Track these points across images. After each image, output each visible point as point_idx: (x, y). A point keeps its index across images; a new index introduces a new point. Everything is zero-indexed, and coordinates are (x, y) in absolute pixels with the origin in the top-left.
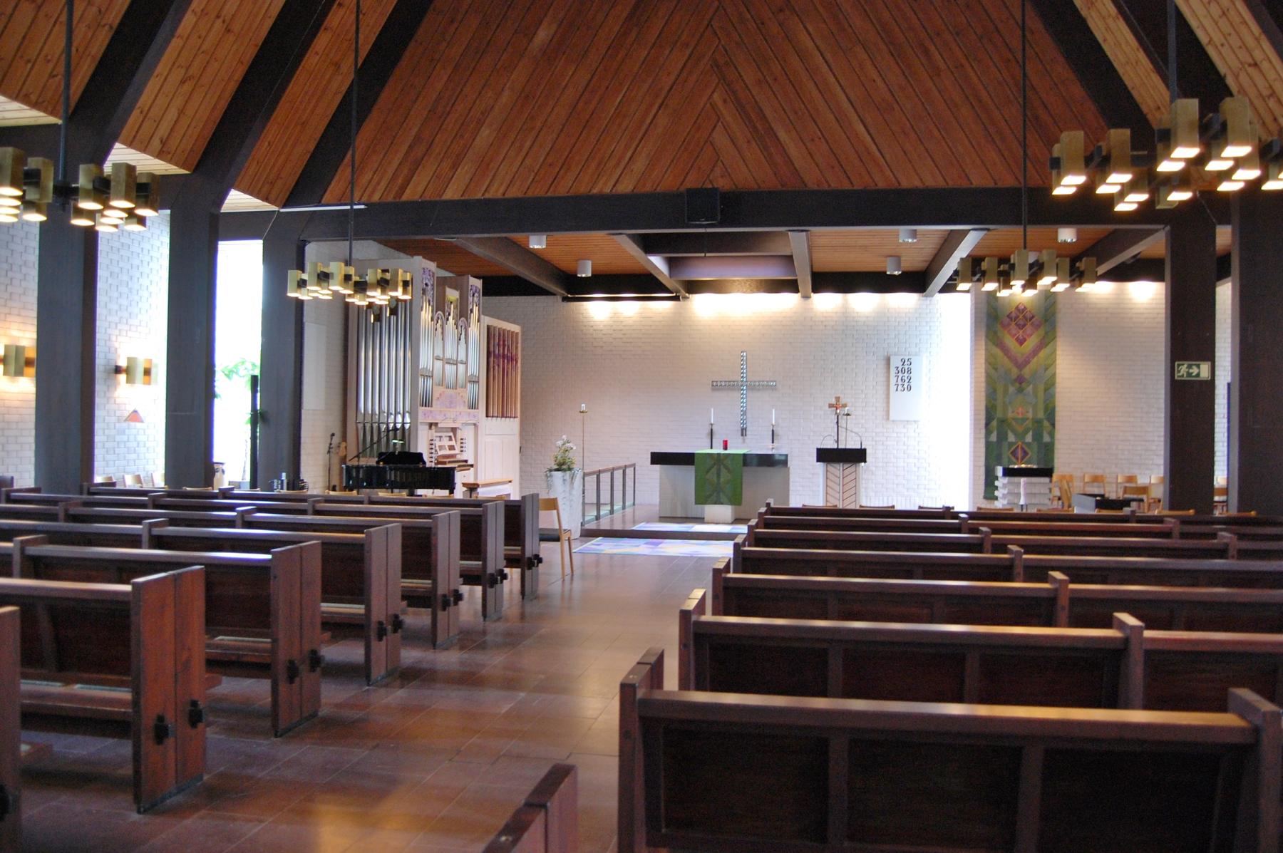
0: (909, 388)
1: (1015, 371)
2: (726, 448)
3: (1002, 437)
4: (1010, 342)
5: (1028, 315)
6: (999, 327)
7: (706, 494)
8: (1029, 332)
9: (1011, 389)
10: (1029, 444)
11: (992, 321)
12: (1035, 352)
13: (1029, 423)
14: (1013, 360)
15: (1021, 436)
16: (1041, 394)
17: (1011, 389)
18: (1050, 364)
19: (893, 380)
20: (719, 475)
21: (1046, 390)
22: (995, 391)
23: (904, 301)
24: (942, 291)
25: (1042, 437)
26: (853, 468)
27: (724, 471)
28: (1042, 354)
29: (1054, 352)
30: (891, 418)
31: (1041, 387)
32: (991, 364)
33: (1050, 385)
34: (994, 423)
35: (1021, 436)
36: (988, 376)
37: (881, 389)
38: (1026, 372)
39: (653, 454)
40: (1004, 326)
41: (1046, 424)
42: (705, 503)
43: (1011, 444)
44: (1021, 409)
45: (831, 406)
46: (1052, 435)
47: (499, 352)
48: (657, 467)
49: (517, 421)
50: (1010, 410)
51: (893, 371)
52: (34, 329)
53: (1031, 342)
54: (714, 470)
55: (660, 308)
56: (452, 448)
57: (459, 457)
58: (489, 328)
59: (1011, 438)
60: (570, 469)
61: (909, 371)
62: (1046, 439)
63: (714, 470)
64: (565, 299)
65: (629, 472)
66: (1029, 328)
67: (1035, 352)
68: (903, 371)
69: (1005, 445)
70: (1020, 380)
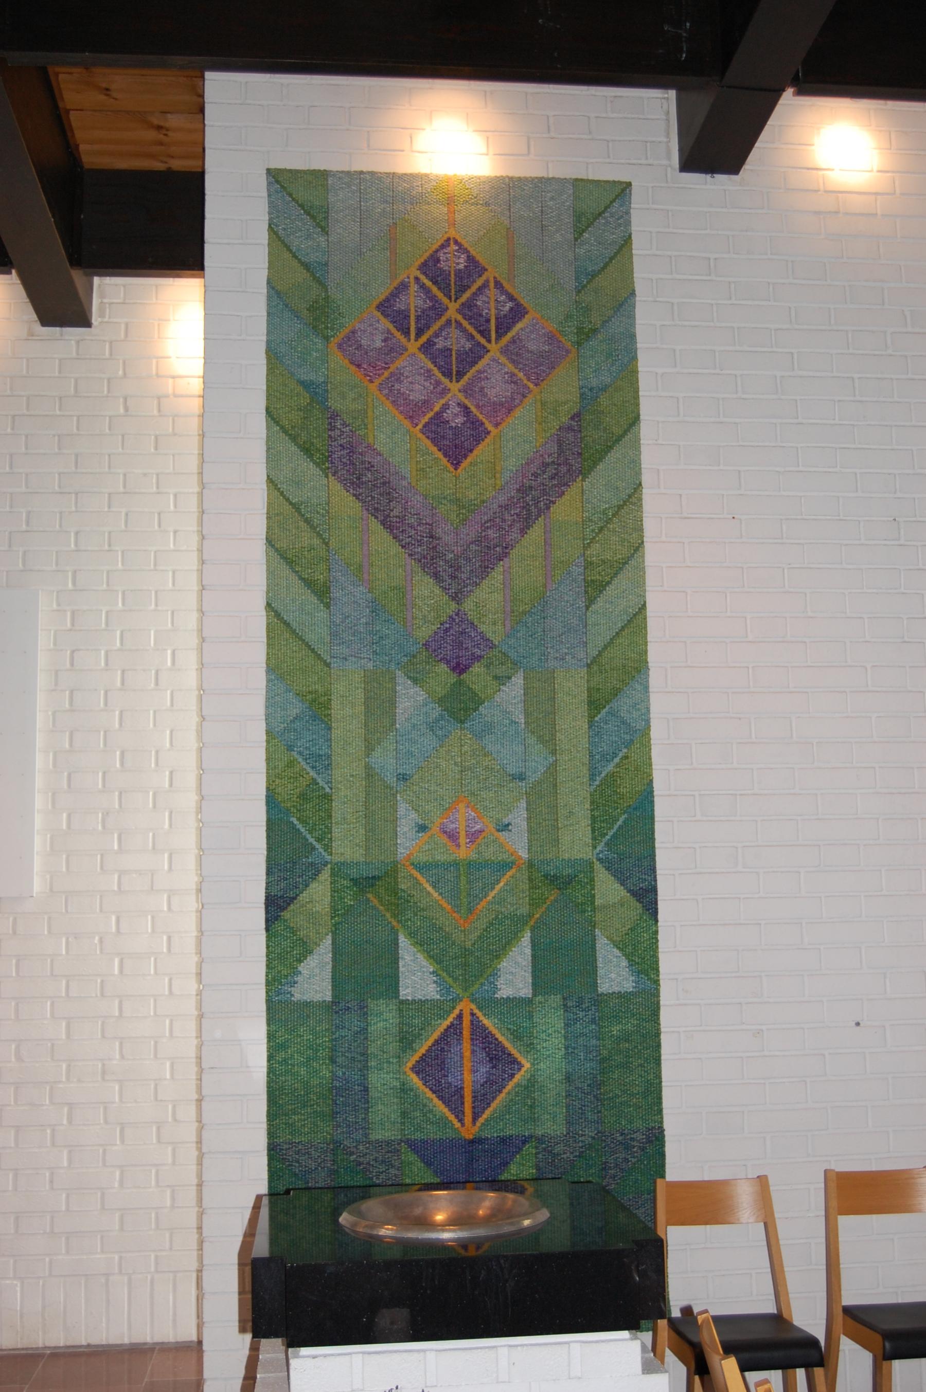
3: (365, 974)
5: (492, 305)
8: (497, 389)
9: (411, 700)
13: (507, 893)
14: (430, 556)
15: (466, 965)
16: (572, 723)
22: (318, 709)
31: (572, 687)
34: (318, 894)
35: (466, 965)
38: (487, 601)
41: (608, 890)
46: (645, 961)
50: (407, 819)
53: (516, 442)
59: (417, 977)
62: (614, 975)
69: (383, 1020)
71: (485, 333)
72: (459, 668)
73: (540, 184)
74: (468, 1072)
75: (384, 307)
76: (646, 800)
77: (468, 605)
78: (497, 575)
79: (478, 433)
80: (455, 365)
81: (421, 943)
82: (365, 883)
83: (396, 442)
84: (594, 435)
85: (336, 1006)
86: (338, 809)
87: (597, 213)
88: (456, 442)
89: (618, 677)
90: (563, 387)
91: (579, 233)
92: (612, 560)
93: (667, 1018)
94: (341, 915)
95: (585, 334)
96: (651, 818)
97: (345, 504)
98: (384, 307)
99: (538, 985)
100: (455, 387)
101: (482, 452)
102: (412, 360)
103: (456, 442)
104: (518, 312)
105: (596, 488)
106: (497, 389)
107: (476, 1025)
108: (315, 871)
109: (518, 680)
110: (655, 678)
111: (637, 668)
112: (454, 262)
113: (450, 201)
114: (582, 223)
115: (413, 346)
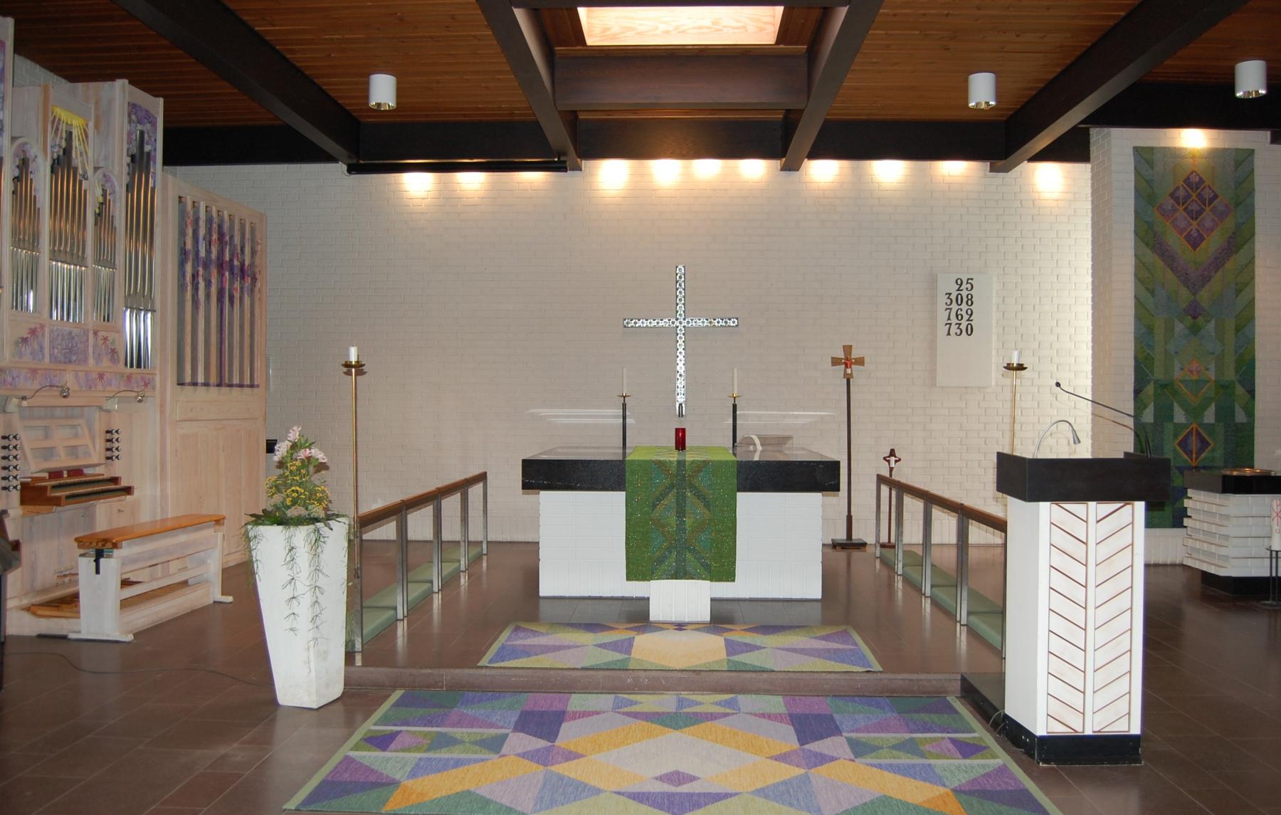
1: (1185, 293)
3: (1164, 414)
5: (1207, 194)
8: (1208, 224)
9: (1179, 328)
12: (1218, 262)
14: (1185, 280)
20: (681, 513)
31: (1230, 324)
34: (1150, 389)
38: (1204, 295)
41: (1239, 390)
43: (1179, 427)
46: (1250, 413)
50: (1177, 365)
52: (1042, 504)
53: (1213, 243)
54: (671, 498)
57: (103, 471)
59: (1180, 416)
61: (970, 300)
62: (1240, 417)
63: (671, 498)
67: (1218, 262)
69: (1169, 427)
72: (1195, 318)
73: (1224, 150)
74: (1194, 443)
75: (1172, 195)
76: (1253, 359)
78: (1207, 287)
79: (1202, 238)
80: (1195, 215)
81: (1181, 406)
82: (1164, 386)
83: (1175, 241)
84: (1241, 239)
85: (1155, 424)
87: (1243, 159)
88: (1195, 243)
89: (1245, 321)
90: (1230, 223)
91: (1237, 167)
92: (1245, 282)
93: (1257, 431)
95: (1238, 204)
96: (1254, 368)
97: (1159, 263)
98: (1172, 195)
99: (1217, 420)
100: (1194, 223)
101: (1203, 245)
102: (1181, 213)
103: (1195, 243)
104: (1216, 196)
105: (1240, 258)
106: (1208, 224)
107: (1197, 432)
109: (1213, 322)
110: (1257, 322)
111: (1251, 319)
112: (1195, 179)
113: (1194, 157)
114: (1238, 164)
115: (1181, 209)
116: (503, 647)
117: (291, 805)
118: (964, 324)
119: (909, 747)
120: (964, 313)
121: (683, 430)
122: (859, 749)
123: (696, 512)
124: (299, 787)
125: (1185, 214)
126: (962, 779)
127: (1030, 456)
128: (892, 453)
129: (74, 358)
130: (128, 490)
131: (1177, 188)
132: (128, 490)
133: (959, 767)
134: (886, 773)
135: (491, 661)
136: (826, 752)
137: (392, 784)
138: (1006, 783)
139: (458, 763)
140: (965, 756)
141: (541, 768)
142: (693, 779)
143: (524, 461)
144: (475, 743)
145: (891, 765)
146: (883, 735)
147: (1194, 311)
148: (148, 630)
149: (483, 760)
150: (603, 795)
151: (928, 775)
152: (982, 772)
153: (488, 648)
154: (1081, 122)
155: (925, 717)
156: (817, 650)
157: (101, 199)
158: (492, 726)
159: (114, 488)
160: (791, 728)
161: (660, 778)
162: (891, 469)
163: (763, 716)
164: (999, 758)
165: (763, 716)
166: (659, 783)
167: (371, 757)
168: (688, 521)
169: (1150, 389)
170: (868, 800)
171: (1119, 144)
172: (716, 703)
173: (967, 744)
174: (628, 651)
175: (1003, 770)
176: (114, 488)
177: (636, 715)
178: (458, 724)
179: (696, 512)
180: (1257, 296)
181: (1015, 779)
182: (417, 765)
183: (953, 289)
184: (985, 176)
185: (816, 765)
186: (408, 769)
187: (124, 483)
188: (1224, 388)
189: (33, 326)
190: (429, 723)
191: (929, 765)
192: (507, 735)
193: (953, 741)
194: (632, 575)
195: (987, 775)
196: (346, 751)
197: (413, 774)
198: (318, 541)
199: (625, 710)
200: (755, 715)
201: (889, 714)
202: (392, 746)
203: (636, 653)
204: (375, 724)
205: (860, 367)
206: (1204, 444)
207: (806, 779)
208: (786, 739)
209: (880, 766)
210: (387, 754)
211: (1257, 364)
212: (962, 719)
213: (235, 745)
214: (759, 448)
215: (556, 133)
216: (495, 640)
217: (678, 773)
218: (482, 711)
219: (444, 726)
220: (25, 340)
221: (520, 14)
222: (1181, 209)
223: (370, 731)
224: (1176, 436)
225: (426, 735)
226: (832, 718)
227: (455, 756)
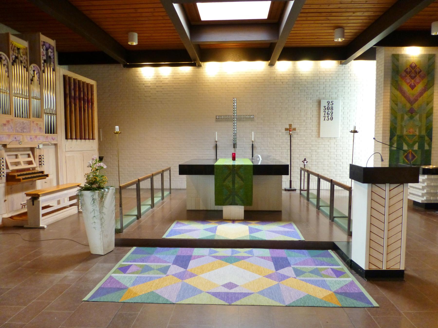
0: (332, 119)
1: (408, 105)
2: (234, 159)
3: (400, 148)
4: (406, 88)
5: (418, 70)
6: (399, 78)
7: (224, 196)
9: (406, 117)
10: (415, 151)
11: (396, 75)
12: (421, 94)
13: (416, 138)
15: (411, 146)
16: (424, 120)
17: (406, 117)
18: (430, 101)
19: (322, 114)
20: (234, 183)
21: (427, 117)
22: (396, 118)
23: (329, 65)
24: (354, 60)
25: (423, 146)
26: (400, 188)
27: (237, 179)
28: (425, 95)
29: (432, 94)
30: (321, 136)
31: (424, 115)
32: (394, 101)
33: (430, 114)
34: (395, 138)
35: (411, 146)
36: (392, 109)
37: (315, 119)
38: (415, 106)
39: (180, 165)
40: (403, 78)
41: (427, 138)
42: (224, 204)
43: (405, 151)
44: (411, 129)
45: (286, 129)
46: (430, 145)
47: (75, 97)
48: (184, 177)
49: (96, 141)
51: (322, 109)
53: (419, 87)
54: (230, 178)
55: (185, 71)
56: (30, 163)
57: (38, 169)
58: (64, 77)
59: (405, 147)
60: (99, 188)
61: (332, 109)
62: (427, 147)
63: (230, 178)
64: (126, 66)
65: (166, 174)
66: (418, 79)
67: (421, 94)
68: (328, 109)
70: (412, 111)
71: (416, 74)
72: (412, 113)
74: (410, 157)
77: (413, 106)
79: (415, 86)
81: (406, 143)
86: (398, 129)
88: (413, 87)
94: (398, 141)
100: (413, 81)
101: (415, 88)
103: (413, 87)
104: (421, 71)
108: (395, 136)
116: (172, 230)
117: (86, 299)
118: (330, 117)
119: (315, 272)
120: (330, 113)
121: (235, 154)
122: (298, 273)
123: (239, 182)
124: (90, 290)
125: (409, 77)
126: (336, 287)
127: (364, 166)
128: (305, 160)
129: (25, 131)
130: (47, 176)
131: (407, 68)
132: (47, 176)
133: (335, 282)
134: (308, 284)
135: (167, 236)
136: (285, 274)
137: (126, 288)
138: (354, 289)
139: (151, 279)
140: (338, 276)
141: (181, 280)
142: (236, 286)
143: (180, 165)
144: (158, 270)
145: (310, 280)
146: (306, 267)
147: (412, 111)
148: (55, 222)
149: (160, 277)
150: (202, 294)
151: (323, 285)
152: (345, 284)
153: (166, 232)
154: (374, 46)
155: (321, 259)
156: (281, 231)
157: (33, 75)
158: (165, 262)
159: (43, 175)
160: (272, 263)
161: (224, 286)
162: (305, 165)
163: (262, 257)
164: (350, 278)
165: (262, 257)
166: (223, 288)
167: (119, 276)
168: (236, 186)
169: (395, 138)
170: (302, 296)
171: (384, 53)
172: (245, 252)
173: (338, 271)
174: (215, 232)
175: (352, 283)
176: (43, 175)
177: (216, 257)
178: (153, 261)
179: (239, 182)
180: (434, 105)
181: (358, 288)
182: (136, 280)
183: (326, 105)
184: (338, 66)
185: (282, 280)
186: (132, 282)
187: (46, 173)
188: (421, 137)
189: (8, 120)
190: (143, 261)
191: (324, 280)
192: (170, 266)
193: (332, 269)
194: (217, 204)
195: (346, 285)
196: (110, 274)
197: (134, 284)
198: (102, 197)
199: (214, 255)
200: (259, 257)
201: (308, 257)
202: (128, 271)
203: (218, 233)
204: (123, 262)
205: (294, 131)
206: (414, 157)
207: (278, 286)
208: (270, 267)
209: (306, 281)
210: (125, 275)
211: (433, 129)
212: (335, 260)
213: (71, 272)
214: (261, 159)
215: (193, 53)
216: (169, 227)
217: (230, 283)
218: (162, 256)
219: (148, 262)
220: (5, 125)
221: (176, 6)
222: (408, 76)
223: (121, 265)
224: (404, 154)
225: (141, 266)
226: (287, 259)
227: (150, 275)
